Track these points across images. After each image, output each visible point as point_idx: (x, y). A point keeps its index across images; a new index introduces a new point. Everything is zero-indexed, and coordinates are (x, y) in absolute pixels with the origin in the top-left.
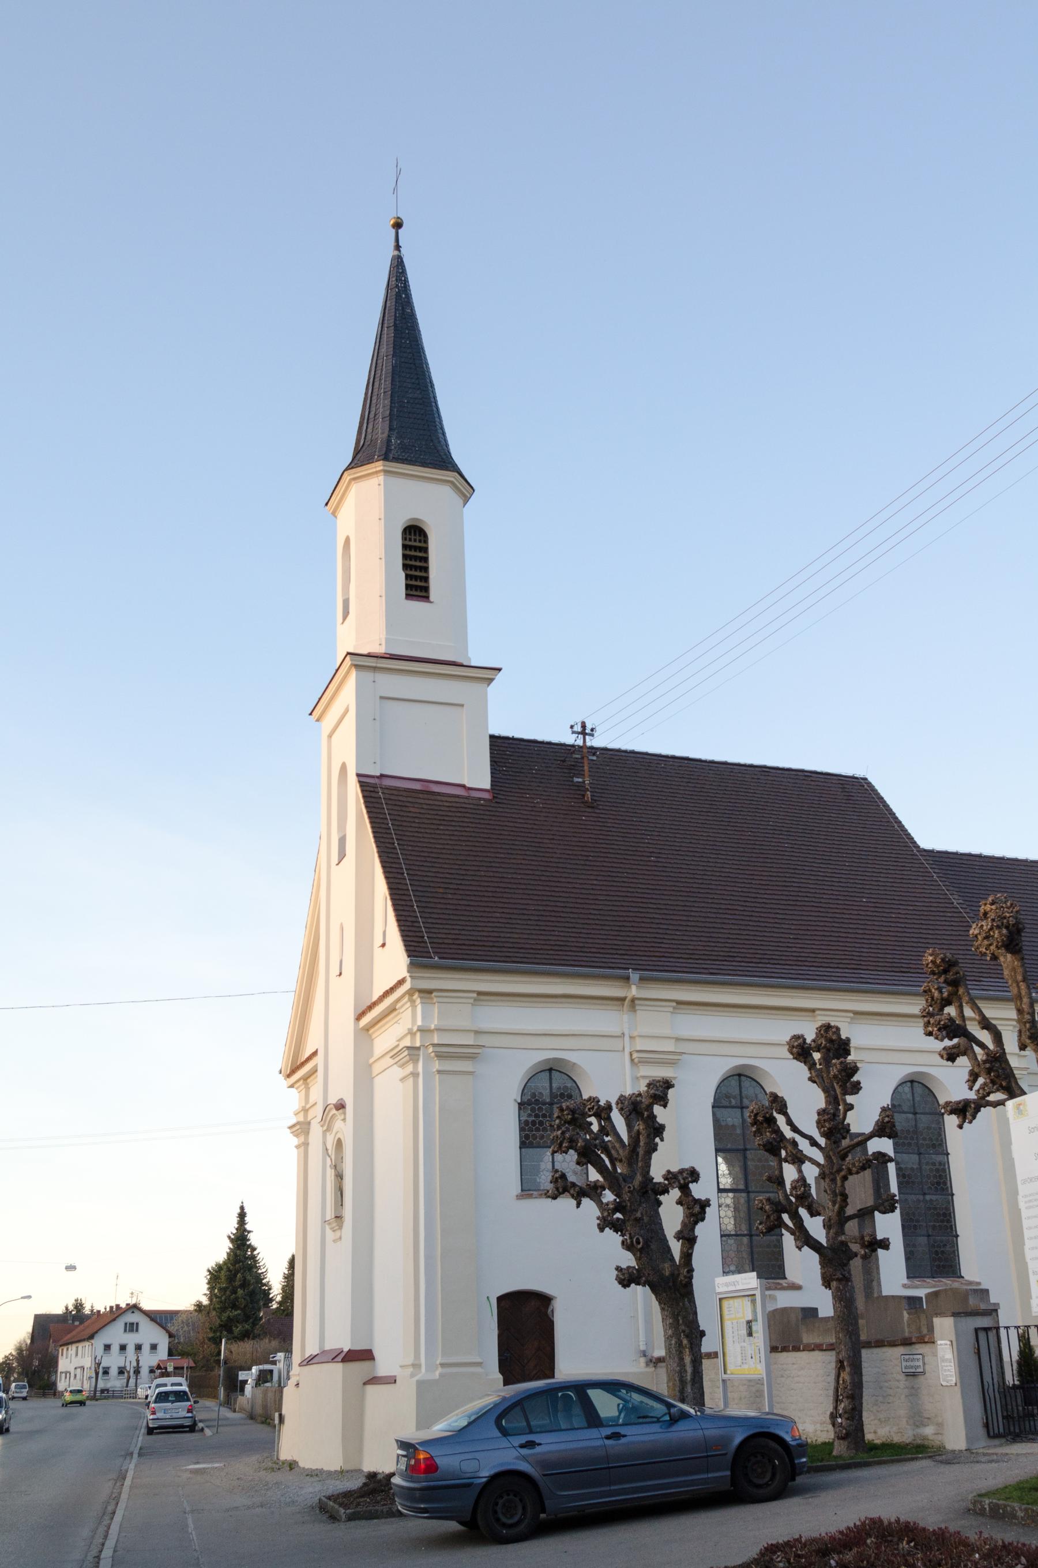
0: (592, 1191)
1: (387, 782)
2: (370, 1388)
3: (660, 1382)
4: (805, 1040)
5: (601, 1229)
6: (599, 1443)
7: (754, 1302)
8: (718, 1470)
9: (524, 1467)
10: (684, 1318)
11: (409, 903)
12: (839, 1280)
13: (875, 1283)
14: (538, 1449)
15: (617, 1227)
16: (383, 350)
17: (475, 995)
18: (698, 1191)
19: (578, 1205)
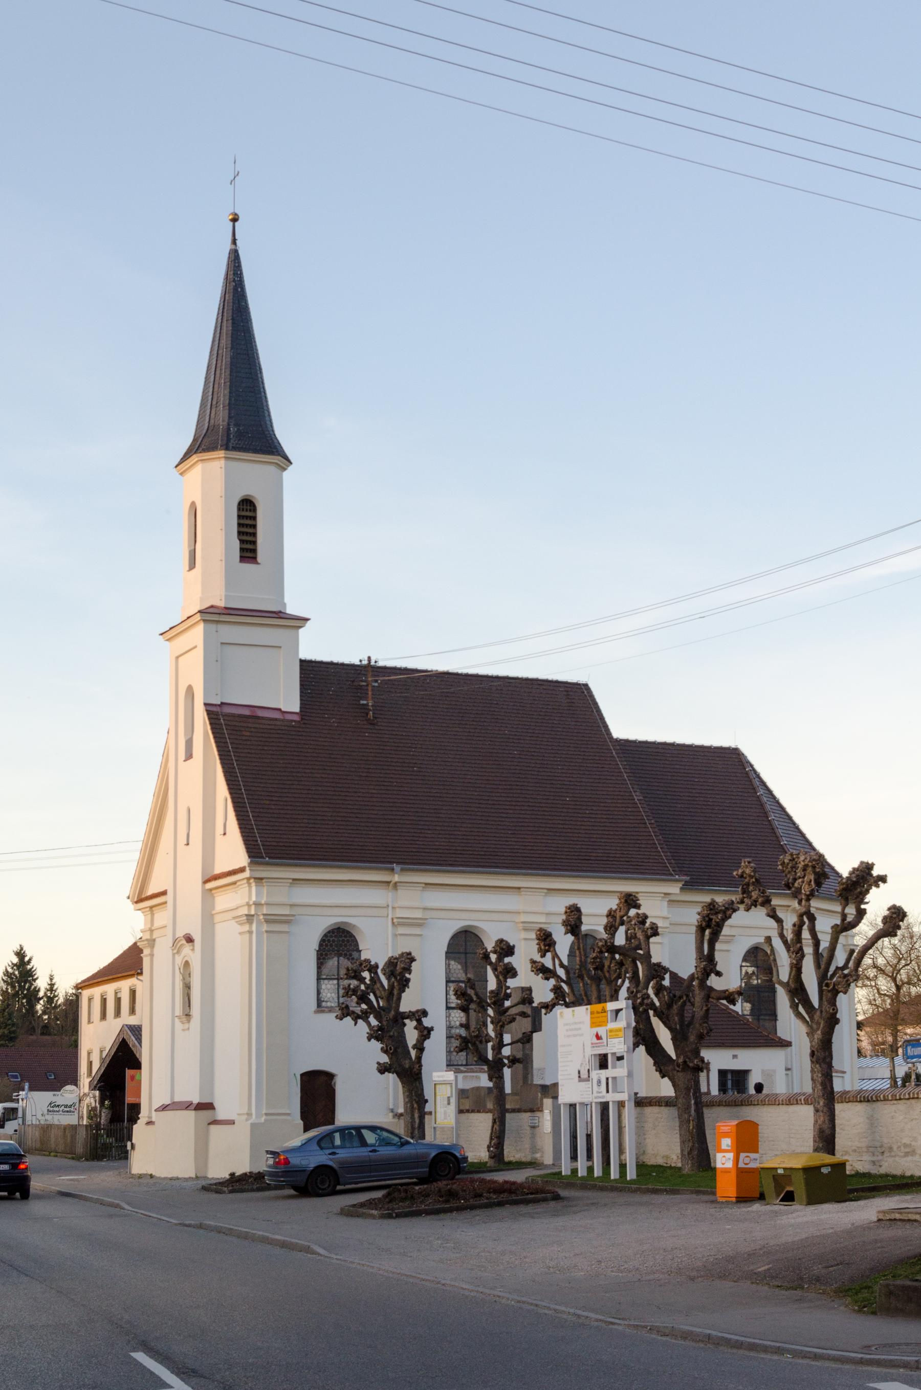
0: (364, 1016)
1: (227, 710)
2: (213, 1127)
3: (400, 1128)
4: (486, 950)
5: (369, 1040)
6: (367, 1154)
7: (451, 1087)
8: (423, 1168)
9: (330, 1163)
10: (416, 1092)
11: (246, 814)
12: (496, 1078)
13: (530, 1075)
14: (337, 1156)
15: (377, 1039)
16: (223, 342)
17: (291, 881)
18: (426, 1022)
19: (356, 1024)
